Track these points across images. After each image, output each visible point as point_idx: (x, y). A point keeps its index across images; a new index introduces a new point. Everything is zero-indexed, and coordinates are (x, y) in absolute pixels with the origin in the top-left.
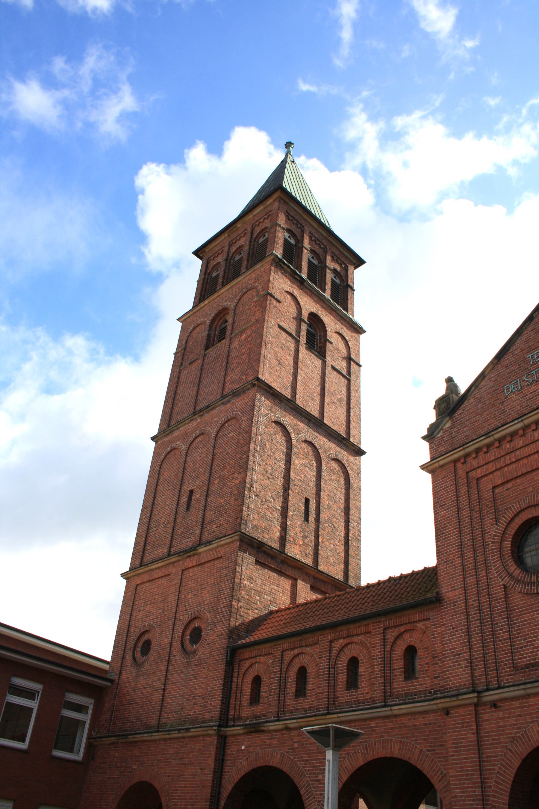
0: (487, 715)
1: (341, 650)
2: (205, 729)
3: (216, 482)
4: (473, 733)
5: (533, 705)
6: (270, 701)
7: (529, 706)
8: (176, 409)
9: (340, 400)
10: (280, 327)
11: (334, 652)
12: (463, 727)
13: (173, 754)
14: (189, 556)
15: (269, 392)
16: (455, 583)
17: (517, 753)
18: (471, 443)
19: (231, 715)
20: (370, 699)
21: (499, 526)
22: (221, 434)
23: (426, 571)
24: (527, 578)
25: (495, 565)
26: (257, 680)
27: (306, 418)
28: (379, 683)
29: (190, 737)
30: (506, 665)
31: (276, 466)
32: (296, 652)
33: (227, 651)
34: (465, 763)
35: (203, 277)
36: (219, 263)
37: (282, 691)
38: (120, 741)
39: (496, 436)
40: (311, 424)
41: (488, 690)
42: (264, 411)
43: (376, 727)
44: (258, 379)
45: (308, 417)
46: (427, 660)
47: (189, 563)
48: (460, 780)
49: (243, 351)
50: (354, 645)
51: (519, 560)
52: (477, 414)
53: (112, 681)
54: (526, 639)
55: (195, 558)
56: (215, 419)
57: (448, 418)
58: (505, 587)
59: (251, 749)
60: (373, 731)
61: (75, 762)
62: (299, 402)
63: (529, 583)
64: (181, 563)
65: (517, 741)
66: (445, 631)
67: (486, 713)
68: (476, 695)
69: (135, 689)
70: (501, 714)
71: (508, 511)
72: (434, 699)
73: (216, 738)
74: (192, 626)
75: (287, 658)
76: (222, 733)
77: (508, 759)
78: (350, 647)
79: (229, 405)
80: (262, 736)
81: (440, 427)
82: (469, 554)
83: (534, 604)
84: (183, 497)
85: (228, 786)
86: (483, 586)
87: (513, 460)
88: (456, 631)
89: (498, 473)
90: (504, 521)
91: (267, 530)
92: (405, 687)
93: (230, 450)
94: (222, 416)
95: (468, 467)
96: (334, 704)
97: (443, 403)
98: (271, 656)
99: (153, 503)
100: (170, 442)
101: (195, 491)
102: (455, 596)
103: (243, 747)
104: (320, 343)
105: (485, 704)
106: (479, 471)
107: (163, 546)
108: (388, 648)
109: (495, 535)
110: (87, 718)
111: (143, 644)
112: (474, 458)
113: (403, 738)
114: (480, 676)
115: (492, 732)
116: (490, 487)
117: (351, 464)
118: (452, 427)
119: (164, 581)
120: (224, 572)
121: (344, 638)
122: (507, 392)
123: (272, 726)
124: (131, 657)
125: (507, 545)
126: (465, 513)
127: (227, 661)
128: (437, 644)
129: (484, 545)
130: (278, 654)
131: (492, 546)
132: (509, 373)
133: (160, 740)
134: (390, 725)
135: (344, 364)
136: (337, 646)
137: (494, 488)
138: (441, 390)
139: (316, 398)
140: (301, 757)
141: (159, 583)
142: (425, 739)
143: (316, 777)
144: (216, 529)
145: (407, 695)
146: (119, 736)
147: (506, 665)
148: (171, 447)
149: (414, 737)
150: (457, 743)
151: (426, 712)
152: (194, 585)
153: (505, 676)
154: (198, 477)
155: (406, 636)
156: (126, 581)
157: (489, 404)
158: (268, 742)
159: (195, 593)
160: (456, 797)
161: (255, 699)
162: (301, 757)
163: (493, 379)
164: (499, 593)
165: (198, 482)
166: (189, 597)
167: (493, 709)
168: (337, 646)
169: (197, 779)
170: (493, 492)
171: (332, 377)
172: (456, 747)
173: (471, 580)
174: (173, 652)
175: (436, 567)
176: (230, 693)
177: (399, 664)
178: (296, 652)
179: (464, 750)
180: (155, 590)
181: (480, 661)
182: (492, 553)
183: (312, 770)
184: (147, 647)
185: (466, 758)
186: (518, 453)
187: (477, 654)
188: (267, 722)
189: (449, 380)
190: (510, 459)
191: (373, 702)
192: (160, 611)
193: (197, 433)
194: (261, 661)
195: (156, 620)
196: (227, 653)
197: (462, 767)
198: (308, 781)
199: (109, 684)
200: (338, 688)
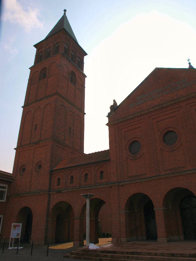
10: (63, 76)
14: (37, 144)
29: (39, 195)
32: (70, 172)
35: (37, 54)
36: (42, 51)
39: (127, 119)
41: (121, 182)
44: (57, 92)
51: (130, 151)
53: (13, 180)
57: (113, 112)
58: (126, 157)
61: (3, 202)
74: (38, 164)
76: (49, 193)
85: (51, 206)
87: (131, 125)
103: (55, 197)
110: (6, 190)
121: (84, 169)
123: (64, 191)
138: (112, 103)
146: (17, 195)
151: (106, 187)
161: (59, 184)
184: (24, 170)
189: (114, 101)
193: (37, 107)
199: (12, 180)
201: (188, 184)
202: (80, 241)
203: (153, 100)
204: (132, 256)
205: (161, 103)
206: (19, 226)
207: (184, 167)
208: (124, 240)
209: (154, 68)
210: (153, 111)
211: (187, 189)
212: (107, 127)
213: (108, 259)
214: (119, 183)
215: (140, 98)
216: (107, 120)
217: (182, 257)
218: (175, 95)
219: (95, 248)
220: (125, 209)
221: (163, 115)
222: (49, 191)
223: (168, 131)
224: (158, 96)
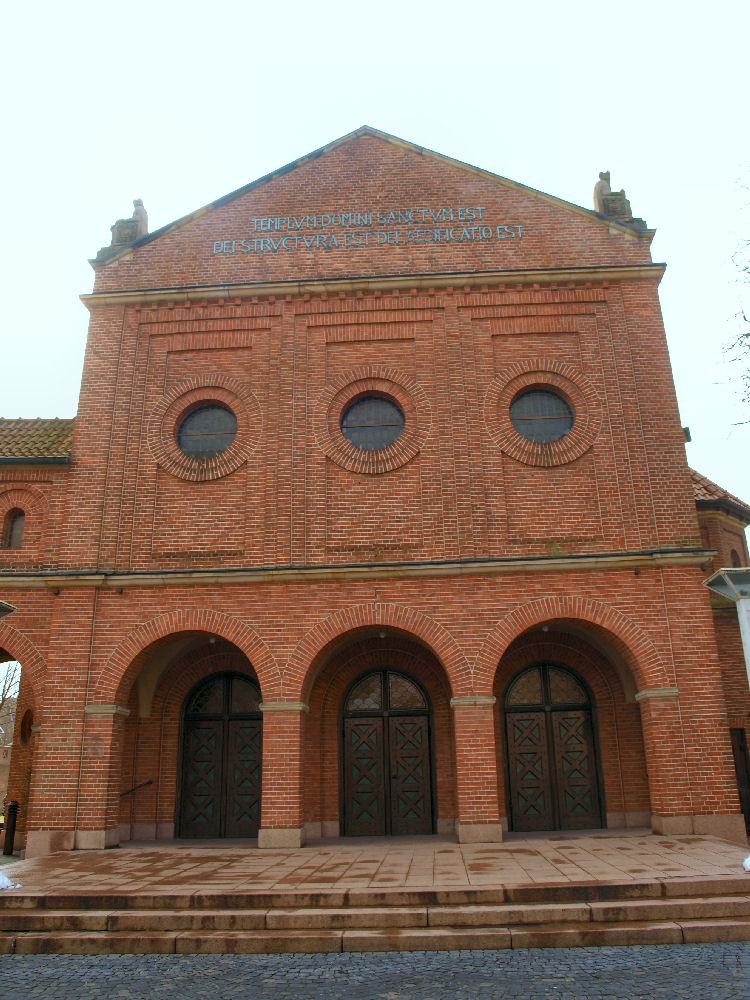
17: (139, 642)
39: (191, 296)
57: (130, 249)
58: (159, 466)
65: (140, 629)
68: (103, 577)
70: (127, 602)
77: (126, 647)
81: (118, 256)
87: (203, 329)
89: (180, 337)
90: (174, 394)
95: (143, 317)
97: (128, 228)
102: (94, 463)
118: (133, 263)
131: (152, 418)
137: (169, 352)
138: (128, 214)
151: (28, 589)
153: (138, 561)
163: (202, 227)
175: (73, 420)
186: (210, 323)
189: (138, 204)
201: (424, 617)
203: (329, 249)
204: (233, 917)
208: (90, 839)
209: (357, 127)
210: (319, 295)
211: (521, 630)
212: (84, 316)
213: (92, 941)
215: (273, 225)
216: (88, 281)
217: (469, 904)
221: (358, 324)
223: (368, 391)
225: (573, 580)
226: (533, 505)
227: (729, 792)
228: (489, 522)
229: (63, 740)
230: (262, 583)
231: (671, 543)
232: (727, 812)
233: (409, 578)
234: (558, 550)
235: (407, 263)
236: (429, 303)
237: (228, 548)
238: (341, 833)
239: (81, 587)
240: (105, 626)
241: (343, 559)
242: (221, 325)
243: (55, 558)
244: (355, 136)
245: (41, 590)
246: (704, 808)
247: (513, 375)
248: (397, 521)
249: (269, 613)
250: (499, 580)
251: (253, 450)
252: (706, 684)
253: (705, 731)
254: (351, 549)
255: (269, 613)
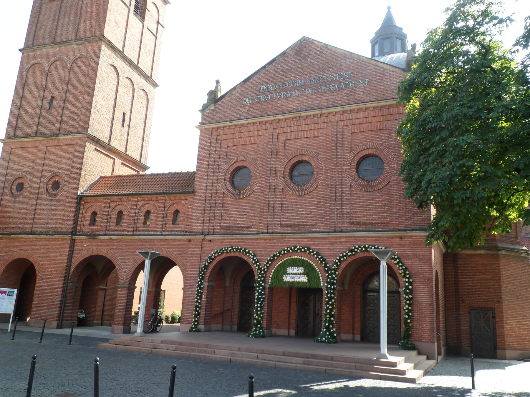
0: (206, 244)
1: (143, 206)
2: (64, 235)
3: (71, 96)
4: (200, 250)
5: (225, 243)
6: (102, 225)
7: (224, 243)
8: (39, 33)
9: (149, 51)
11: (139, 207)
12: (195, 247)
13: (42, 246)
15: (109, 45)
16: (202, 187)
18: (222, 123)
19: (78, 229)
20: (155, 230)
21: (227, 165)
22: (74, 65)
23: (188, 174)
24: (234, 192)
25: (221, 183)
26: (94, 214)
27: (129, 63)
28: (160, 225)
29: (53, 239)
30: (218, 225)
31: (109, 93)
32: (118, 203)
33: (77, 199)
34: (194, 261)
37: (108, 221)
38: (5, 237)
39: (234, 123)
40: (131, 67)
41: (208, 234)
42: (106, 58)
43: (156, 243)
45: (130, 62)
46: (184, 218)
47: (51, 143)
48: (191, 267)
49: (93, 9)
50: (149, 205)
52: (228, 108)
54: (228, 216)
55: (56, 141)
56: (71, 53)
59: (90, 247)
60: (155, 244)
62: (126, 53)
63: (234, 194)
64: (45, 142)
66: (194, 207)
67: (206, 243)
68: (203, 236)
69: (14, 210)
70: (212, 245)
71: (232, 160)
72: (185, 235)
73: (70, 240)
74: (53, 180)
75: (112, 206)
76: (73, 238)
78: (147, 205)
79: (81, 46)
80: (97, 241)
81: (209, 108)
82: (211, 175)
83: (234, 203)
84: (46, 99)
85: (76, 262)
86: (214, 191)
87: (240, 137)
88: (199, 208)
90: (229, 164)
91: (101, 131)
92: (172, 227)
93: (82, 78)
94: (76, 52)
96: (136, 230)
97: (212, 94)
98: (103, 203)
99: (22, 97)
100: (34, 57)
101: (55, 97)
104: (142, 9)
105: (207, 240)
106: (223, 136)
107: (32, 128)
108: (166, 209)
109: (224, 169)
111: (18, 185)
112: (221, 130)
113: (168, 249)
114: (206, 228)
115: (207, 250)
116: (226, 146)
117: (151, 93)
118: (214, 110)
119: (32, 150)
120: (77, 154)
122: (245, 102)
124: (9, 191)
125: (228, 175)
126: (212, 155)
127: (77, 203)
128: (189, 212)
129: (218, 172)
130: (108, 203)
131: (222, 174)
132: (247, 92)
133: (33, 239)
134: (163, 243)
135: (155, 26)
136: (140, 204)
139: (135, 49)
140: (118, 252)
141: (29, 150)
142: (178, 250)
143: (124, 261)
144: (70, 127)
145: (172, 231)
147: (218, 225)
148: (35, 61)
149: (173, 249)
150: (192, 253)
151: (180, 240)
152: (55, 157)
153: (217, 230)
154: (57, 89)
155: (175, 205)
156: (2, 144)
157: (235, 105)
158: (100, 244)
159: (56, 161)
160: (188, 273)
161: (93, 222)
162: (118, 252)
164: (221, 195)
165: (57, 92)
166: (51, 163)
167: (209, 242)
168: (140, 204)
169: (58, 259)
170: (227, 149)
171: (147, 34)
172: (191, 255)
173: (209, 187)
174: (40, 193)
176: (78, 219)
177: (170, 217)
178: (118, 203)
179: (195, 256)
180: (26, 154)
181: (208, 222)
182: (221, 177)
183: (123, 258)
185: (195, 259)
186: (242, 134)
187: (207, 219)
188: (99, 235)
190: (238, 136)
191: (157, 232)
192: (30, 167)
193: (56, 58)
194: (97, 205)
195: (28, 173)
196: (77, 199)
197: (193, 263)
198: (120, 263)
200: (138, 224)
202: (124, 325)
205: (299, 108)
206: (13, 292)
207: (314, 226)
209: (300, 38)
214: (205, 235)
218: (324, 98)
219: (118, 303)
220: (208, 280)
221: (297, 131)
222: (72, 235)
224: (297, 94)
225: (374, 241)
226: (362, 208)
227: (430, 334)
228: (342, 215)
229: (192, 293)
230: (257, 239)
231: (418, 226)
232: (428, 342)
233: (309, 238)
234: (370, 227)
235: (317, 102)
236: (326, 120)
237: (247, 225)
238: (296, 335)
239: (197, 239)
240: (205, 254)
241: (287, 229)
242: (246, 134)
243: (189, 229)
244: (300, 42)
245: (185, 240)
246: (419, 339)
247: (358, 151)
248: (308, 215)
249: (259, 250)
250: (344, 240)
251: (256, 187)
252: (426, 288)
253: (422, 307)
254: (290, 226)
255: (259, 250)
